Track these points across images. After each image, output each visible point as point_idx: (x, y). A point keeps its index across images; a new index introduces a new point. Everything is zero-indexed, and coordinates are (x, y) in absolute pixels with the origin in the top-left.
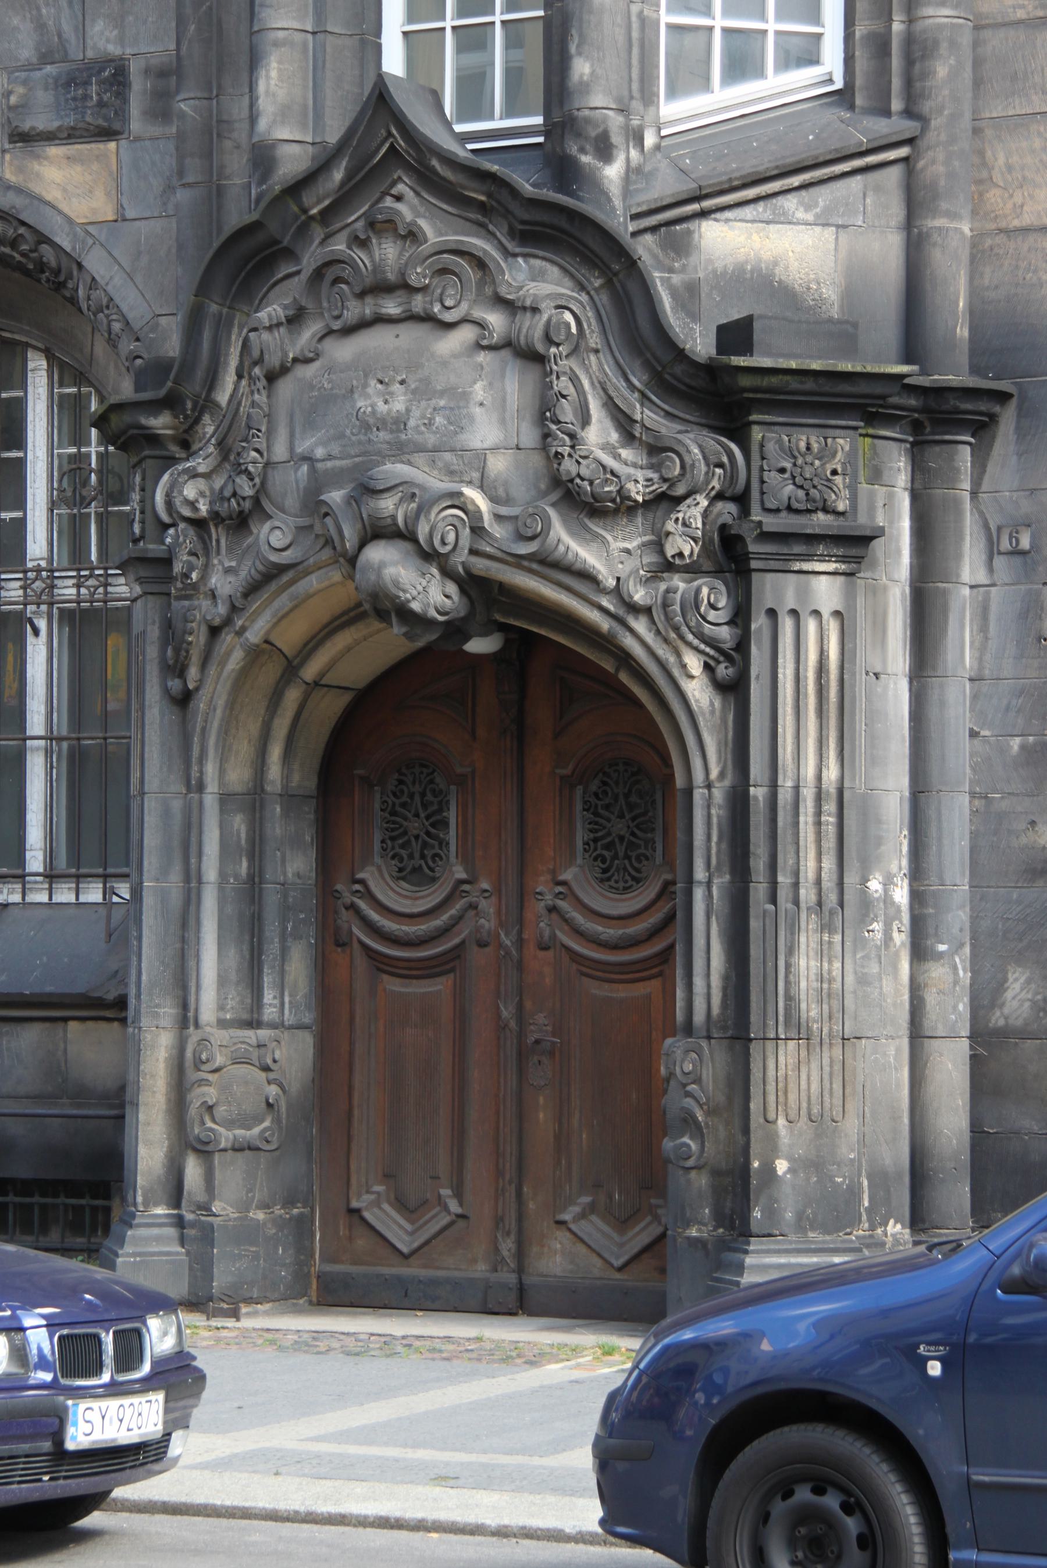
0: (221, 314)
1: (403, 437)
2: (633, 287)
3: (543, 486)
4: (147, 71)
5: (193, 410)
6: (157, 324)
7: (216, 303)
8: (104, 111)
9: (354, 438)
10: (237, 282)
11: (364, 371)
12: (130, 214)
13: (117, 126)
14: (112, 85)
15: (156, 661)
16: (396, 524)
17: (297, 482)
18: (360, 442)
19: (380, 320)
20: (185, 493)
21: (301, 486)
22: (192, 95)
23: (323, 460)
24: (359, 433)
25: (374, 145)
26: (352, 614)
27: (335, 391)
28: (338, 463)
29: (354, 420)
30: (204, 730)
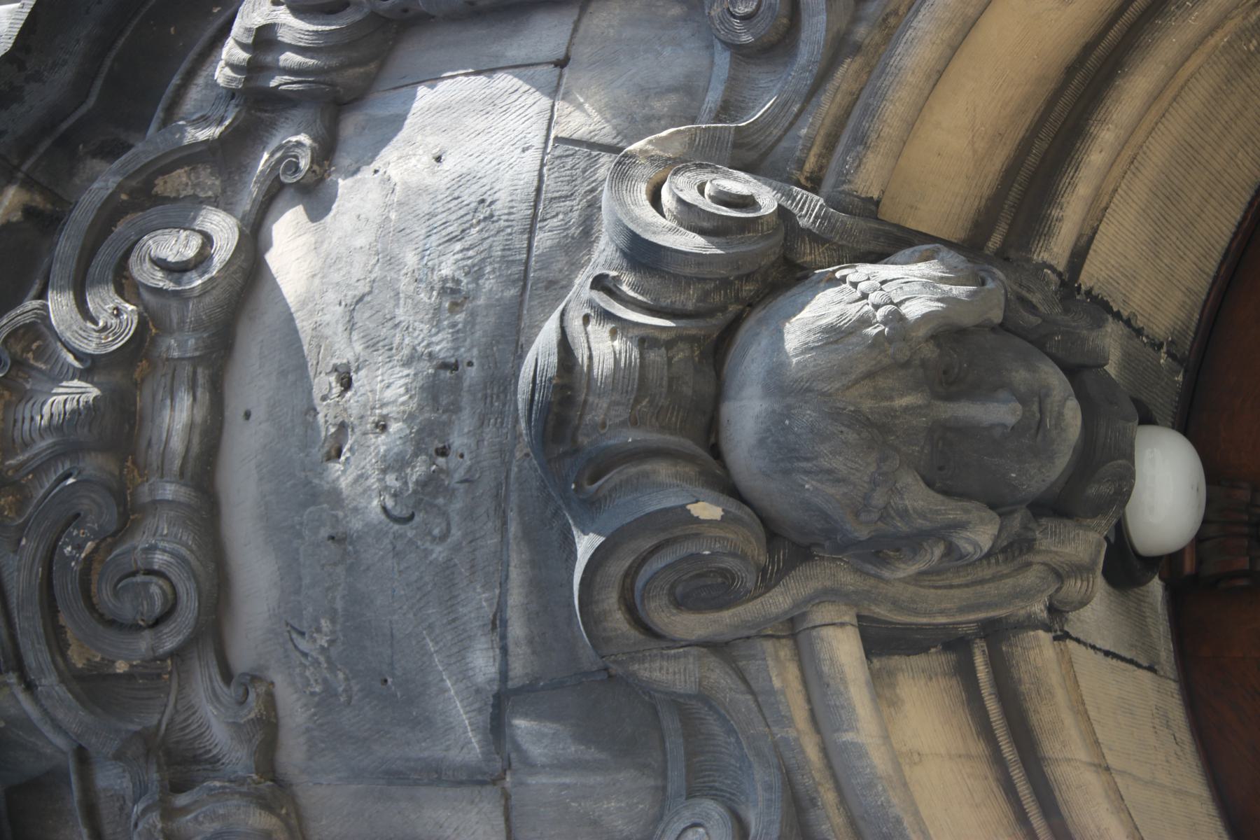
9: (456, 534)
11: (304, 505)
16: (671, 342)
17: (563, 766)
18: (469, 514)
19: (204, 468)
21: (573, 750)
23: (504, 650)
24: (444, 514)
27: (339, 605)
28: (516, 597)
29: (409, 531)
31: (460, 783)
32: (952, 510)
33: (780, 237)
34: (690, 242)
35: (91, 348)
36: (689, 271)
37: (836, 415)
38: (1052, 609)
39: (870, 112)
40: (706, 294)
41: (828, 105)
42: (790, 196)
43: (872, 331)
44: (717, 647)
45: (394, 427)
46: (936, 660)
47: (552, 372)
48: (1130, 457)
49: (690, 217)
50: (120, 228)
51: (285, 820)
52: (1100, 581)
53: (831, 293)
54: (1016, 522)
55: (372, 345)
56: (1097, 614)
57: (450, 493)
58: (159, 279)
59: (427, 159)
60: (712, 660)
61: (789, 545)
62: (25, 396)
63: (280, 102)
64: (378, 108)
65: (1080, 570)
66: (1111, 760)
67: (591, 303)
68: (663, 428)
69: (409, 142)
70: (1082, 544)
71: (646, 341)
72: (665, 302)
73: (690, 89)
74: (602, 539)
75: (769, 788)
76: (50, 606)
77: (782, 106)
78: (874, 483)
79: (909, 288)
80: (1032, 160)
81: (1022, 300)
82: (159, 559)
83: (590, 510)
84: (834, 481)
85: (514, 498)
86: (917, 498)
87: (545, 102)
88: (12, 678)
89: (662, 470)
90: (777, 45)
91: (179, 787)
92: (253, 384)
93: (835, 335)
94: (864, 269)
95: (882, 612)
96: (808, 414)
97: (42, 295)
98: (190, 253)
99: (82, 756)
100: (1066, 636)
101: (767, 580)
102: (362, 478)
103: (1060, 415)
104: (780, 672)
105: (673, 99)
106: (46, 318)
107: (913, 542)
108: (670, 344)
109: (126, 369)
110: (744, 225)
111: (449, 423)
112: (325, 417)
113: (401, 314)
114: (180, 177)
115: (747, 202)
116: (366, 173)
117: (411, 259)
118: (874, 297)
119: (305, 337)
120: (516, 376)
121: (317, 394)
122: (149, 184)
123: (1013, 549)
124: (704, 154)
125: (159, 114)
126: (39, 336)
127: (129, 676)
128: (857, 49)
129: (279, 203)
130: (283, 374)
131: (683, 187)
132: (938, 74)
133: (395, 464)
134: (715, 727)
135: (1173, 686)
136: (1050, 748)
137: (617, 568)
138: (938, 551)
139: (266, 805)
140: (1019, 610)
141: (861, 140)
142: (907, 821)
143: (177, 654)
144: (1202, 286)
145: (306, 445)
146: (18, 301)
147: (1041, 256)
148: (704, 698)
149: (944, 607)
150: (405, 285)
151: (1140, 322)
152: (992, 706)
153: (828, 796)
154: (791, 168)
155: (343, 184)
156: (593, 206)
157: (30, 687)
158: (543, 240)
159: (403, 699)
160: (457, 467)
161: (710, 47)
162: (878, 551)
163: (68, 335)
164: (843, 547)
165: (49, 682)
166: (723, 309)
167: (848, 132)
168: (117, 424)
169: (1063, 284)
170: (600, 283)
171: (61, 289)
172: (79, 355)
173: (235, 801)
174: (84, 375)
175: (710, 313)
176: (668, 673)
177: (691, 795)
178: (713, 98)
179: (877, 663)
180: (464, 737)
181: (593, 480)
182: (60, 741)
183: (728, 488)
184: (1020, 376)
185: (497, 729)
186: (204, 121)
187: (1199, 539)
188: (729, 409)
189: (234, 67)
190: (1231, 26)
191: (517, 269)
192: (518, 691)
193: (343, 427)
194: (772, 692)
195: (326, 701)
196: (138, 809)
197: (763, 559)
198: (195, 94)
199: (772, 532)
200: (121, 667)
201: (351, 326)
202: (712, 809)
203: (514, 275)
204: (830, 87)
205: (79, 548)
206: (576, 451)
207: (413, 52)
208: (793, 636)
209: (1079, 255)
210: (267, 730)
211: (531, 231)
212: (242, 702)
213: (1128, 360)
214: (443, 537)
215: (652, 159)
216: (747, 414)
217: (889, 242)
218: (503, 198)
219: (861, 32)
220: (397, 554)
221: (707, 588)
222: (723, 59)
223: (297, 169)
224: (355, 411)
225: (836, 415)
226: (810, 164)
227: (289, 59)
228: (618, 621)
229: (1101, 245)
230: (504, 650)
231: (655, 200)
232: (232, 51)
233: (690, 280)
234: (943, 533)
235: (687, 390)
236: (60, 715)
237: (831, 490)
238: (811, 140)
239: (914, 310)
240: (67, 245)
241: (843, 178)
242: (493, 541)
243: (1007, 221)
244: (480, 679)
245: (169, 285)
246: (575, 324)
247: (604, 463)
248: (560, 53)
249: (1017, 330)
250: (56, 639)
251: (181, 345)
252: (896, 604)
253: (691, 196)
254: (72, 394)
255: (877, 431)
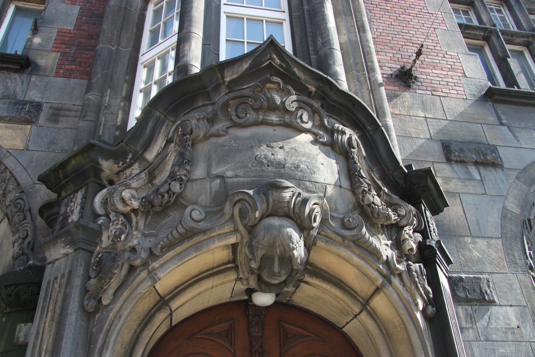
0: (160, 117)
1: (283, 171)
2: (377, 137)
3: (350, 207)
4: (51, 108)
5: (131, 159)
6: (34, 187)
7: (159, 112)
8: (30, 114)
9: (253, 168)
10: (173, 105)
11: (258, 141)
12: (30, 148)
13: (34, 120)
14: (35, 108)
15: (79, 287)
17: (211, 189)
18: (256, 171)
19: (264, 123)
20: (123, 194)
21: (214, 190)
22: (95, 94)
23: (232, 177)
24: (257, 166)
25: (264, 59)
26: (215, 270)
28: (241, 179)
29: (254, 160)
30: (108, 331)
31: (208, 170)
32: (258, 259)
33: (308, 227)
34: (307, 211)
35: (286, 103)
36: (302, 210)
37: (275, 238)
38: (241, 278)
39: (332, 244)
40: (297, 213)
41: (333, 236)
42: (316, 229)
43: (291, 244)
44: (232, 216)
45: (273, 157)
46: (231, 257)
47: (283, 185)
48: (269, 293)
49: (312, 210)
50: (308, 108)
51: (202, 139)
52: (246, 287)
53: (298, 237)
54: (256, 272)
55: (288, 152)
56: (241, 287)
57: (261, 167)
58: (299, 114)
59: (322, 162)
60: (230, 216)
61: (251, 230)
62: (278, 92)
63: (332, 136)
64: (332, 153)
65: (248, 284)
66: (214, 289)
67: (296, 192)
68: (272, 206)
69: (325, 159)
70: (253, 284)
71: (289, 203)
72: (296, 206)
73: (336, 210)
74: (252, 195)
75: (207, 226)
76: (240, 97)
77: (333, 227)
78: (263, 245)
79: (299, 251)
80: (324, 274)
81: (298, 272)
82: (248, 115)
83: (257, 193)
84: (263, 238)
85: (259, 179)
86: (260, 253)
87: (333, 184)
88: (228, 91)
89: (265, 206)
90: (344, 226)
91: (208, 120)
92: (280, 131)
93: (290, 238)
94: (303, 243)
95: (239, 247)
96: (275, 233)
97: (296, 94)
98: (304, 120)
99: (214, 104)
100: (236, 281)
101: (245, 226)
102: (263, 151)
103: (276, 279)
104: (228, 228)
105: (334, 207)
106: (292, 95)
107: (252, 253)
108: (288, 207)
109: (283, 109)
110: (311, 220)
111: (273, 166)
112: (274, 144)
113: (293, 158)
114: (318, 118)
115: (315, 221)
116: (319, 151)
117: (304, 159)
118: (297, 245)
119: (289, 140)
120: (282, 179)
121: (279, 143)
122: (316, 113)
123: (251, 271)
124: (324, 213)
125: (329, 114)
126: (288, 94)
127: (228, 111)
128: (344, 241)
129: (314, 136)
130: (282, 137)
131: (317, 209)
132: (339, 256)
133: (266, 157)
134: (218, 217)
135: (228, 300)
136: (215, 278)
137: (246, 198)
138: (251, 257)
139: (204, 136)
140: (241, 272)
141: (327, 242)
142: (201, 252)
143: (231, 119)
144: (302, 305)
145: (269, 141)
146: (295, 90)
147: (306, 276)
148: (223, 214)
149: (241, 258)
150: (299, 158)
151: (295, 294)
152: (223, 267)
153: (206, 237)
154: (321, 229)
155: (317, 147)
156: (314, 192)
157: (226, 94)
158: (308, 183)
159: (223, 159)
160: (265, 168)
161: (344, 214)
162: (250, 246)
163: (289, 99)
164: (251, 239)
165: (227, 97)
166: (295, 217)
167: (328, 239)
168: (273, 108)
169: (301, 280)
170: (299, 194)
171: (297, 98)
172: (285, 101)
173: (205, 130)
174: (282, 102)
175: (294, 214)
176: (228, 207)
177: (206, 212)
178: (335, 214)
179: (230, 246)
180: (215, 171)
181: (263, 193)
182: (216, 100)
183: (262, 218)
184: (283, 272)
185: (217, 176)
186: (328, 122)
187: (255, 305)
188: (276, 218)
189: (338, 127)
190: (349, 309)
191: (302, 179)
192: (224, 181)
193: (273, 147)
194: (224, 227)
195: (223, 145)
196: (204, 113)
197: (249, 225)
198: (333, 121)
199: (254, 226)
200: (229, 110)
201: (291, 149)
202: (203, 216)
203: (300, 178)
204: (337, 236)
205: (251, 102)
206: (268, 190)
207: (342, 159)
208: (235, 231)
209: (306, 283)
210: (218, 135)
211: (309, 181)
212: (223, 131)
213: (287, 292)
214: (252, 166)
215: (323, 203)
216: (275, 221)
217: (308, 247)
218: (315, 176)
219: (347, 242)
220: (249, 158)
221: (243, 215)
222: (341, 216)
223: (320, 138)
224: (275, 149)
225: (275, 238)
226: (322, 233)
227: (340, 137)
228: (237, 198)
229: (309, 286)
230: (232, 177)
231: (315, 204)
232: (341, 127)
233: (300, 211)
234: (254, 258)
235: (280, 210)
236: (221, 99)
237: (261, 237)
238: (327, 233)
239: (295, 252)
240: (305, 99)
241: (320, 239)
242: (252, 175)
243: (312, 269)
244: (227, 173)
245: (298, 116)
246: (292, 189)
247: (266, 195)
248: (342, 186)
249: (292, 272)
250: (234, 98)
251: (287, 119)
252: (241, 250)
253: (316, 210)
254: (278, 100)
255: (272, 246)
